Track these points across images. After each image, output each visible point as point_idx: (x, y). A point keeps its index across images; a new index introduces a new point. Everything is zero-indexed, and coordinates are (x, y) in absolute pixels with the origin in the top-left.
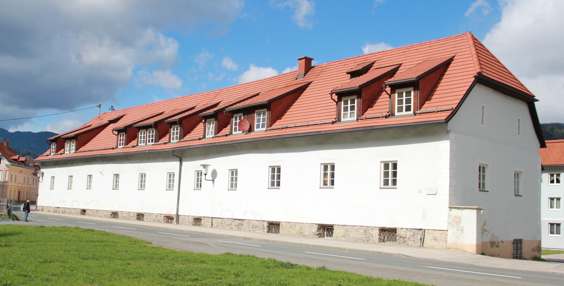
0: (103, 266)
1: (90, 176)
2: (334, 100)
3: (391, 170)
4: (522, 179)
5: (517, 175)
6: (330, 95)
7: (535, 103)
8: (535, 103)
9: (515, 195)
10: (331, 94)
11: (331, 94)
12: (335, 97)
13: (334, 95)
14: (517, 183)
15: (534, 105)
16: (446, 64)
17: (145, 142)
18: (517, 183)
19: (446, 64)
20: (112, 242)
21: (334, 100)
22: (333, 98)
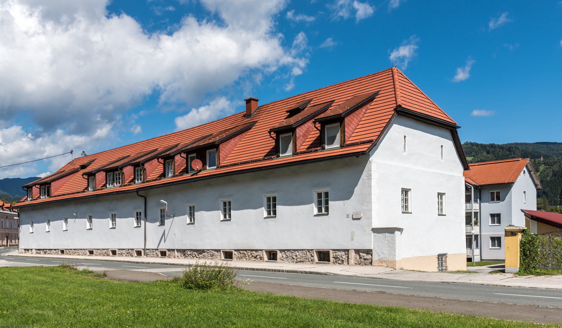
0: (60, 315)
1: (441, 195)
2: (272, 138)
3: (323, 199)
4: (406, 138)
5: (405, 192)
6: (268, 134)
7: (458, 130)
8: (458, 130)
9: (439, 215)
10: (270, 132)
11: (270, 132)
12: (274, 135)
13: (272, 133)
14: (441, 204)
15: (456, 132)
16: (377, 94)
17: (486, 194)
18: (441, 204)
19: (377, 94)
20: (88, 285)
21: (272, 138)
22: (272, 136)
